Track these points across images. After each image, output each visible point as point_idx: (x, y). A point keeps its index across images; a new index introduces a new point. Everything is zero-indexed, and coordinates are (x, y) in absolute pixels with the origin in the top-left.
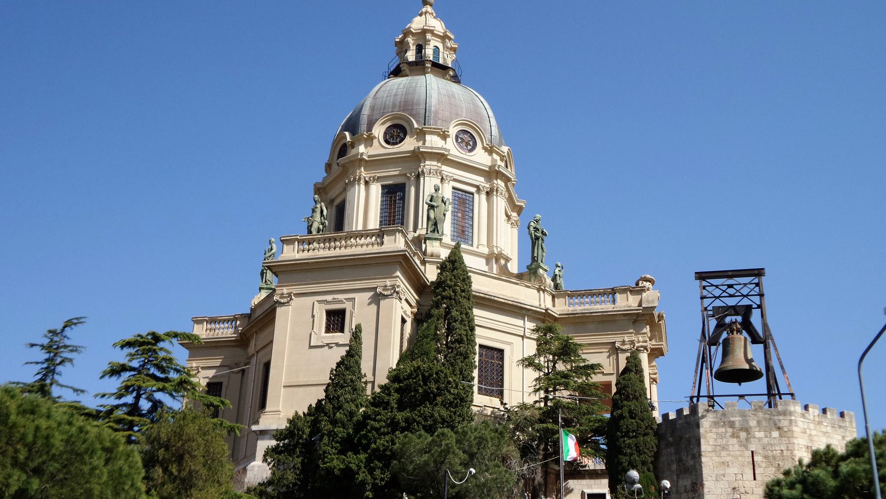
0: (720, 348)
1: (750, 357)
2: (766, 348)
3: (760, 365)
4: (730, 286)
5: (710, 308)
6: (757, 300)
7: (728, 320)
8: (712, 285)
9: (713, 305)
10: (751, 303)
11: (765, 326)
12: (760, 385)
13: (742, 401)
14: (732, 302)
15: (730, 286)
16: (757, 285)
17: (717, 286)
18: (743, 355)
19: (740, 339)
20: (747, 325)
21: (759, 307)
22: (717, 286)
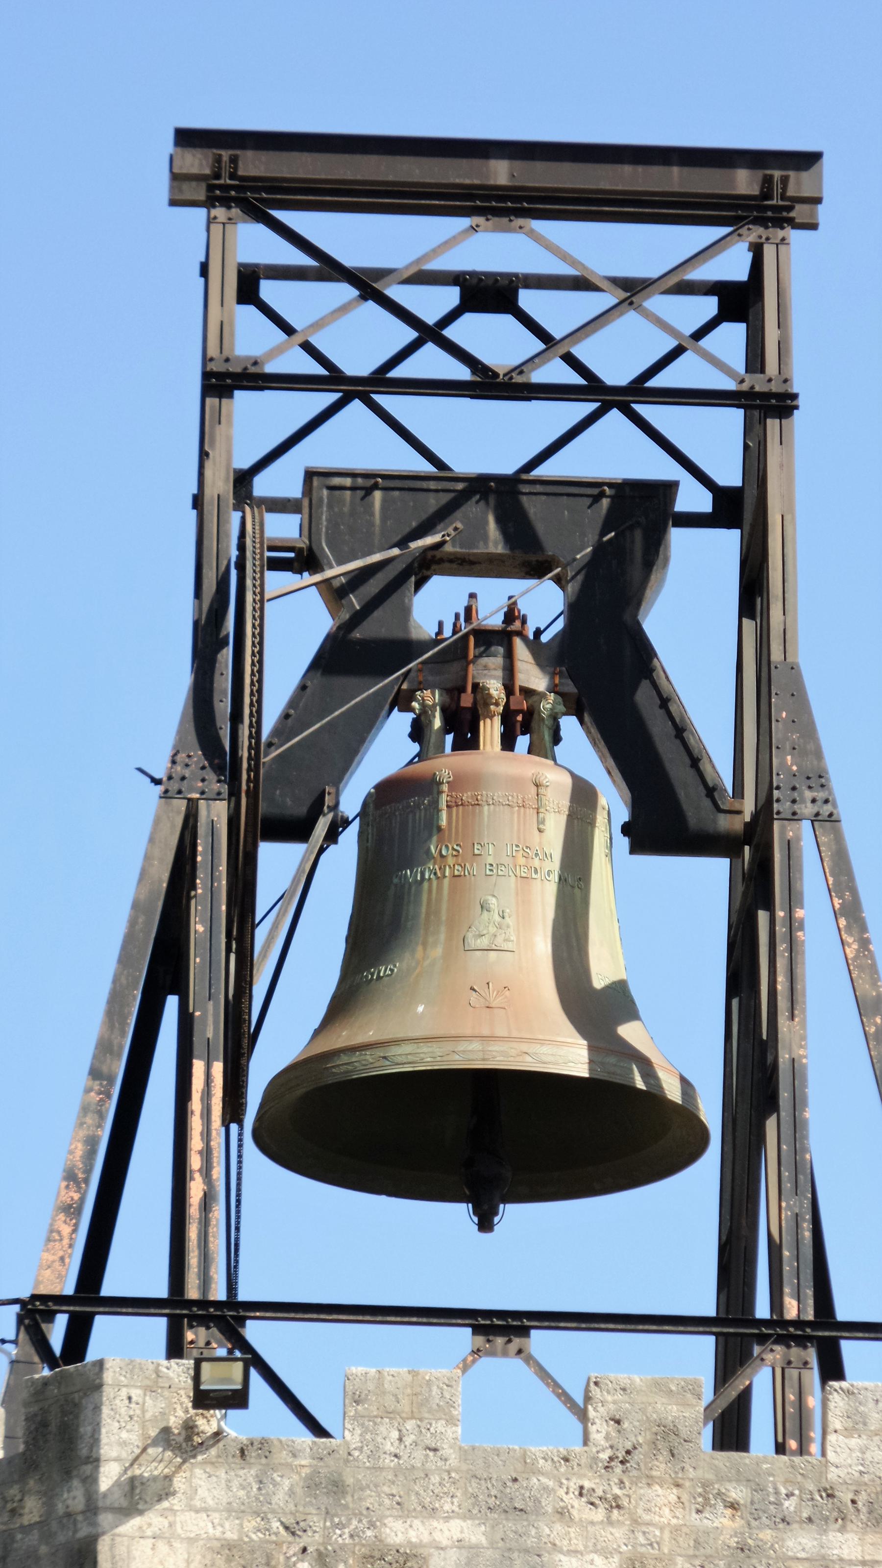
0: (342, 862)
1: (604, 968)
2: (756, 892)
3: (683, 1051)
4: (490, 294)
5: (282, 481)
6: (716, 441)
7: (435, 607)
8: (329, 269)
9: (316, 452)
10: (657, 467)
11: (767, 683)
12: (655, 1237)
13: (502, 1369)
14: (485, 440)
15: (490, 294)
16: (739, 301)
17: (368, 285)
18: (542, 946)
19: (533, 798)
20: (607, 673)
21: (738, 508)
22: (368, 285)
